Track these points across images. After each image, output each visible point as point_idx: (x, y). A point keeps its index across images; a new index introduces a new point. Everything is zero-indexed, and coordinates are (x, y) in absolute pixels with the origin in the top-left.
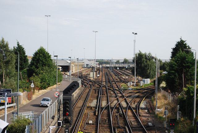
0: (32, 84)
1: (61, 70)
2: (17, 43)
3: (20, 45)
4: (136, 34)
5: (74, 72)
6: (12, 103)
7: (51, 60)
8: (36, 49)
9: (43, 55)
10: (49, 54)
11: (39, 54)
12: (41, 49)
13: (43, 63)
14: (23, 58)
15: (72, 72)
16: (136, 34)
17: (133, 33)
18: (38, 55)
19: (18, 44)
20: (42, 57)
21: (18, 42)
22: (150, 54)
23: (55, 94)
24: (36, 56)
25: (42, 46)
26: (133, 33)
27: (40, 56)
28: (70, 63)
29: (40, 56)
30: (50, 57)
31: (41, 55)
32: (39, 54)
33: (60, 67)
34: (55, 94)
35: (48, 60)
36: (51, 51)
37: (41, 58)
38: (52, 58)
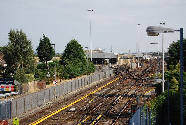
0: (49, 73)
1: (108, 62)
2: (43, 36)
3: (46, 37)
4: (164, 24)
5: (121, 64)
6: (15, 91)
7: (82, 51)
8: (68, 41)
9: (75, 46)
10: (80, 46)
11: (71, 46)
12: (72, 41)
13: (75, 54)
14: (49, 49)
15: (120, 64)
16: (164, 24)
17: (161, 23)
18: (70, 47)
19: (44, 36)
20: (73, 50)
21: (44, 35)
22: (21, 33)
23: (53, 82)
24: (68, 48)
25: (74, 38)
26: (161, 23)
27: (71, 48)
28: (117, 56)
29: (71, 48)
30: (81, 48)
31: (72, 46)
32: (71, 46)
33: (108, 60)
34: (53, 82)
35: (80, 52)
36: (83, 43)
37: (72, 50)
38: (84, 49)
